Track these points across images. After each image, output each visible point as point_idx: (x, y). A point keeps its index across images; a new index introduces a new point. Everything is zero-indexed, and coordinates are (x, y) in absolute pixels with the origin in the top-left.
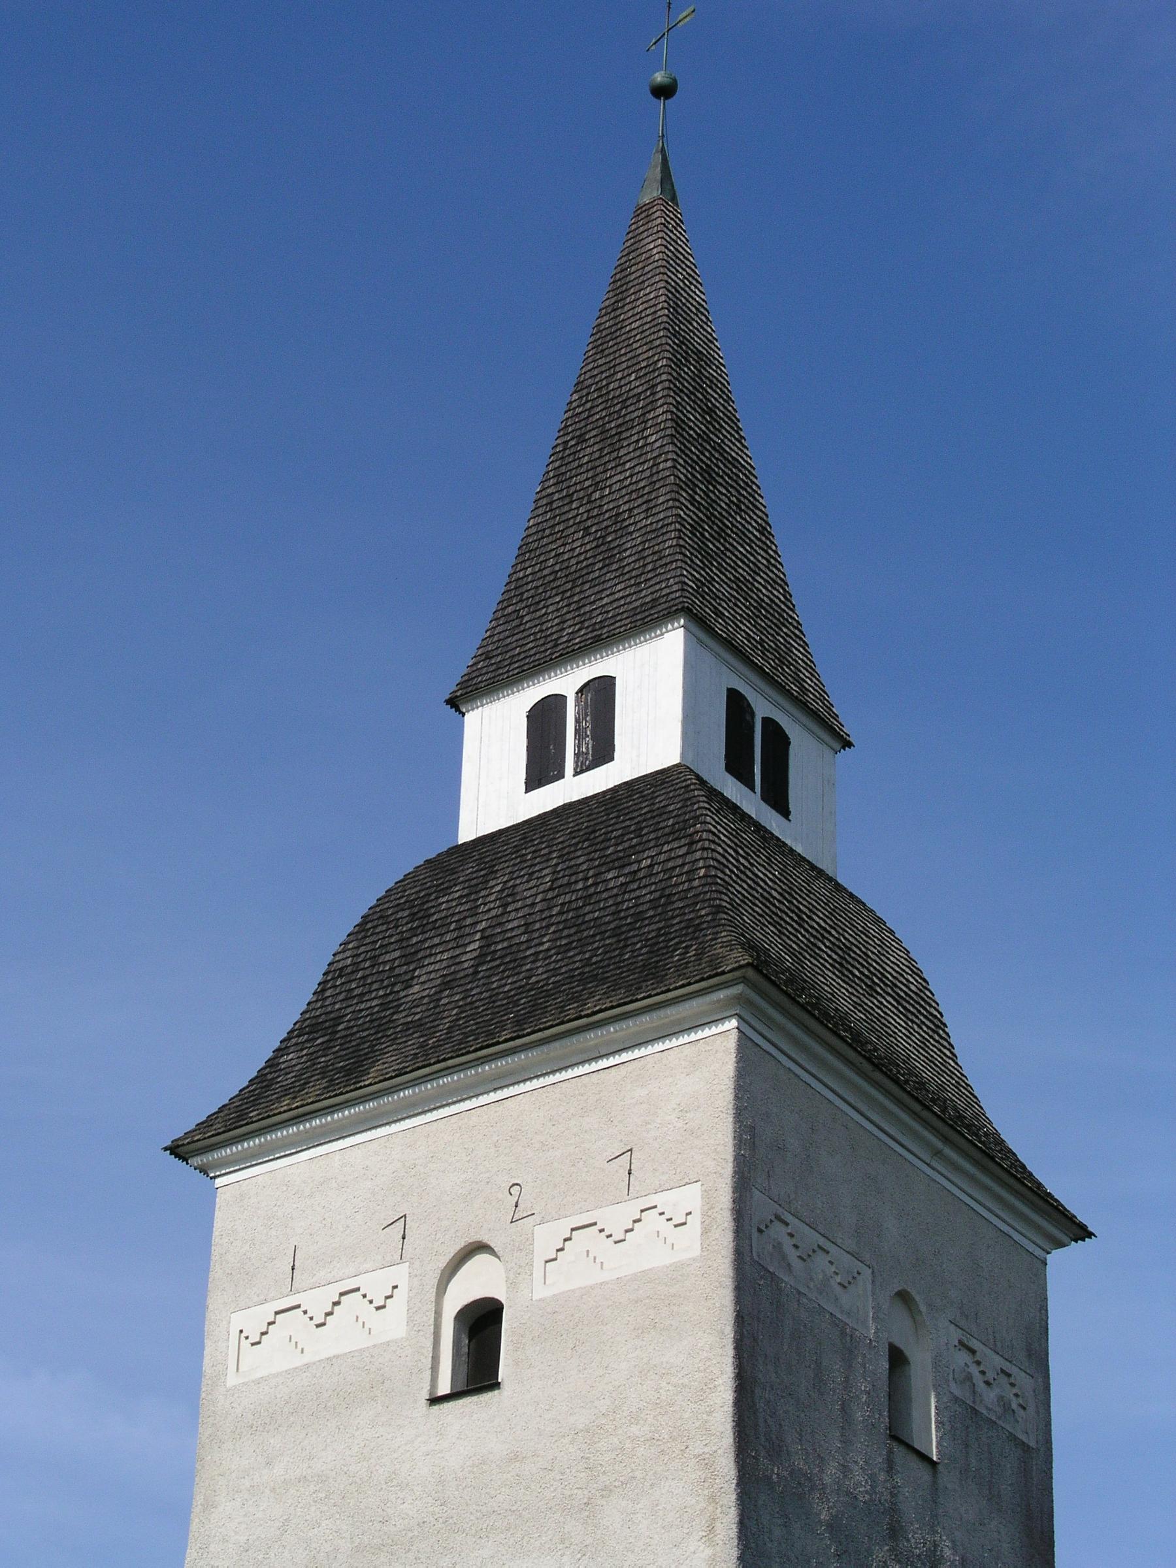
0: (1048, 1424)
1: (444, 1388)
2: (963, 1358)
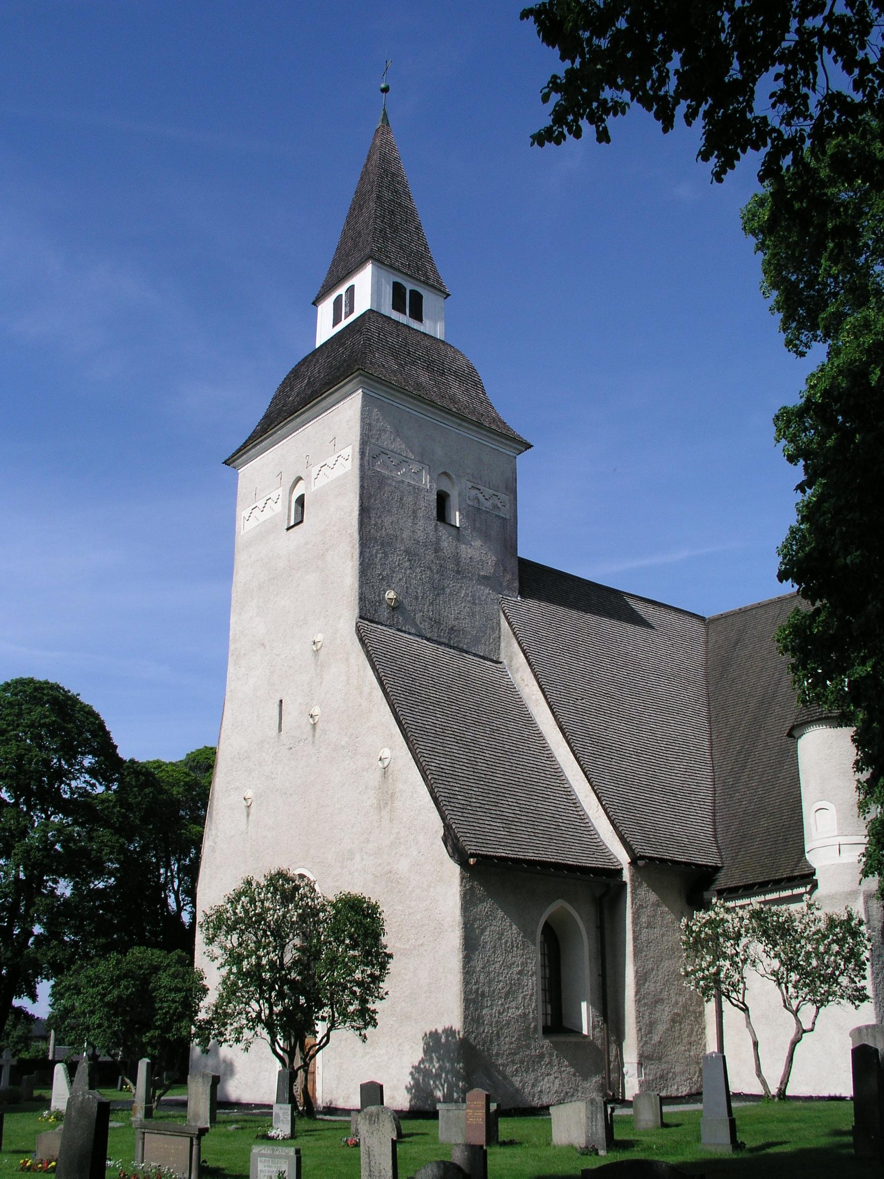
0: (516, 510)
1: (292, 523)
2: (474, 492)
